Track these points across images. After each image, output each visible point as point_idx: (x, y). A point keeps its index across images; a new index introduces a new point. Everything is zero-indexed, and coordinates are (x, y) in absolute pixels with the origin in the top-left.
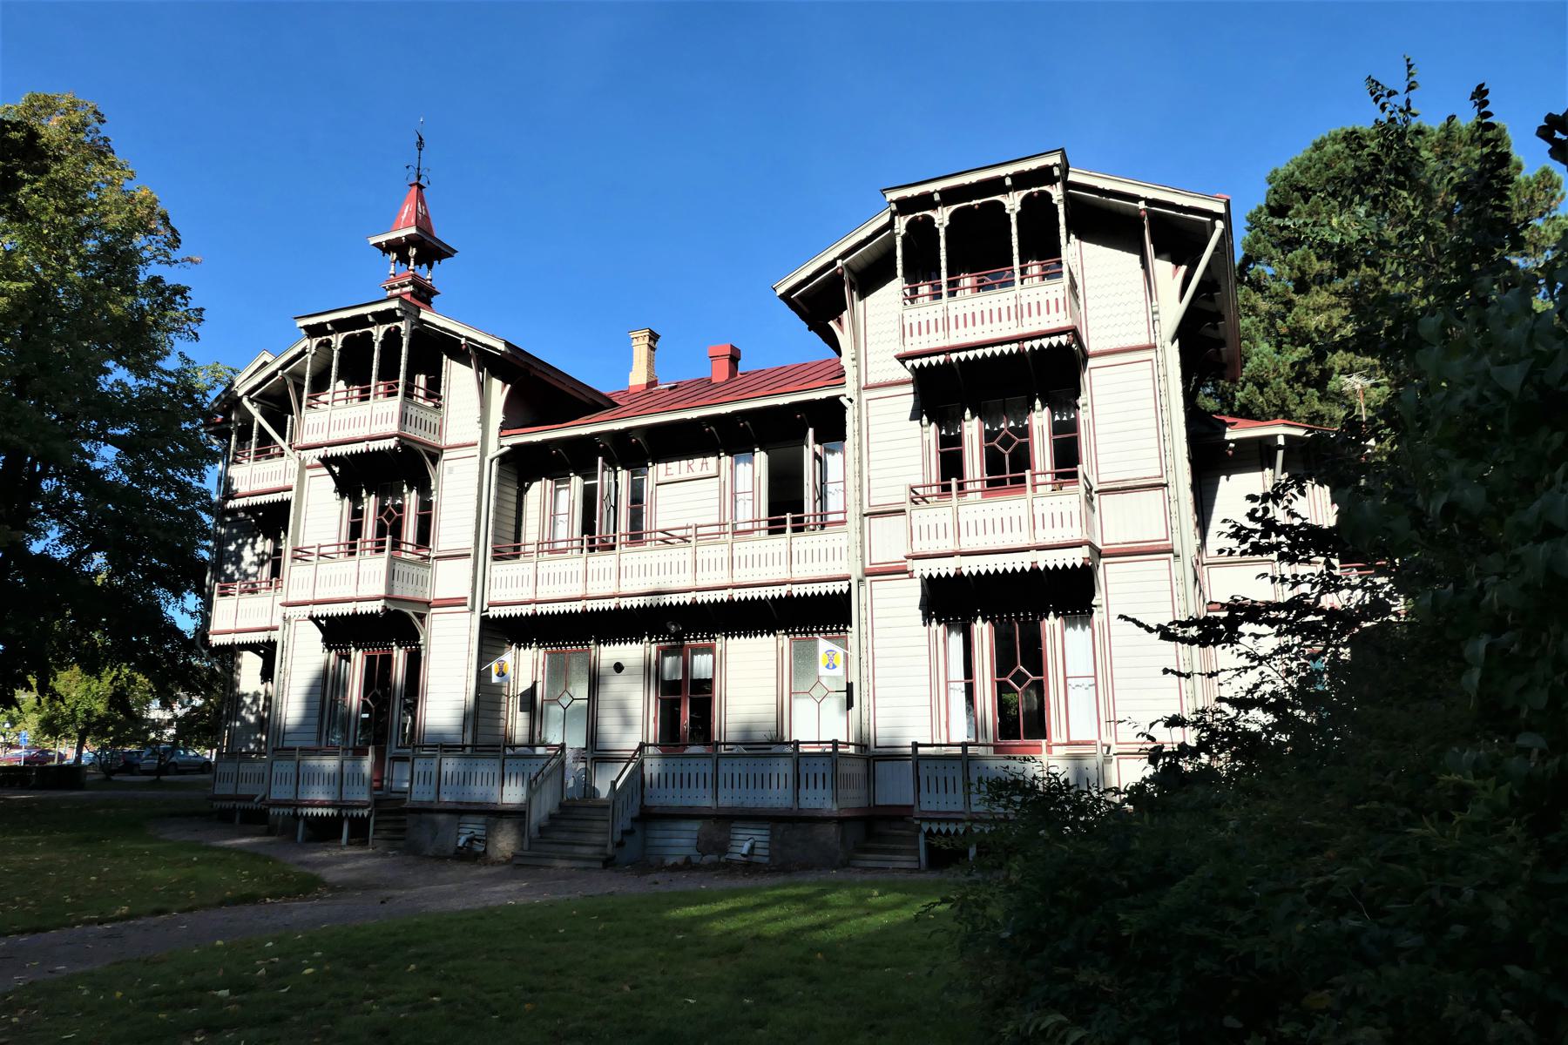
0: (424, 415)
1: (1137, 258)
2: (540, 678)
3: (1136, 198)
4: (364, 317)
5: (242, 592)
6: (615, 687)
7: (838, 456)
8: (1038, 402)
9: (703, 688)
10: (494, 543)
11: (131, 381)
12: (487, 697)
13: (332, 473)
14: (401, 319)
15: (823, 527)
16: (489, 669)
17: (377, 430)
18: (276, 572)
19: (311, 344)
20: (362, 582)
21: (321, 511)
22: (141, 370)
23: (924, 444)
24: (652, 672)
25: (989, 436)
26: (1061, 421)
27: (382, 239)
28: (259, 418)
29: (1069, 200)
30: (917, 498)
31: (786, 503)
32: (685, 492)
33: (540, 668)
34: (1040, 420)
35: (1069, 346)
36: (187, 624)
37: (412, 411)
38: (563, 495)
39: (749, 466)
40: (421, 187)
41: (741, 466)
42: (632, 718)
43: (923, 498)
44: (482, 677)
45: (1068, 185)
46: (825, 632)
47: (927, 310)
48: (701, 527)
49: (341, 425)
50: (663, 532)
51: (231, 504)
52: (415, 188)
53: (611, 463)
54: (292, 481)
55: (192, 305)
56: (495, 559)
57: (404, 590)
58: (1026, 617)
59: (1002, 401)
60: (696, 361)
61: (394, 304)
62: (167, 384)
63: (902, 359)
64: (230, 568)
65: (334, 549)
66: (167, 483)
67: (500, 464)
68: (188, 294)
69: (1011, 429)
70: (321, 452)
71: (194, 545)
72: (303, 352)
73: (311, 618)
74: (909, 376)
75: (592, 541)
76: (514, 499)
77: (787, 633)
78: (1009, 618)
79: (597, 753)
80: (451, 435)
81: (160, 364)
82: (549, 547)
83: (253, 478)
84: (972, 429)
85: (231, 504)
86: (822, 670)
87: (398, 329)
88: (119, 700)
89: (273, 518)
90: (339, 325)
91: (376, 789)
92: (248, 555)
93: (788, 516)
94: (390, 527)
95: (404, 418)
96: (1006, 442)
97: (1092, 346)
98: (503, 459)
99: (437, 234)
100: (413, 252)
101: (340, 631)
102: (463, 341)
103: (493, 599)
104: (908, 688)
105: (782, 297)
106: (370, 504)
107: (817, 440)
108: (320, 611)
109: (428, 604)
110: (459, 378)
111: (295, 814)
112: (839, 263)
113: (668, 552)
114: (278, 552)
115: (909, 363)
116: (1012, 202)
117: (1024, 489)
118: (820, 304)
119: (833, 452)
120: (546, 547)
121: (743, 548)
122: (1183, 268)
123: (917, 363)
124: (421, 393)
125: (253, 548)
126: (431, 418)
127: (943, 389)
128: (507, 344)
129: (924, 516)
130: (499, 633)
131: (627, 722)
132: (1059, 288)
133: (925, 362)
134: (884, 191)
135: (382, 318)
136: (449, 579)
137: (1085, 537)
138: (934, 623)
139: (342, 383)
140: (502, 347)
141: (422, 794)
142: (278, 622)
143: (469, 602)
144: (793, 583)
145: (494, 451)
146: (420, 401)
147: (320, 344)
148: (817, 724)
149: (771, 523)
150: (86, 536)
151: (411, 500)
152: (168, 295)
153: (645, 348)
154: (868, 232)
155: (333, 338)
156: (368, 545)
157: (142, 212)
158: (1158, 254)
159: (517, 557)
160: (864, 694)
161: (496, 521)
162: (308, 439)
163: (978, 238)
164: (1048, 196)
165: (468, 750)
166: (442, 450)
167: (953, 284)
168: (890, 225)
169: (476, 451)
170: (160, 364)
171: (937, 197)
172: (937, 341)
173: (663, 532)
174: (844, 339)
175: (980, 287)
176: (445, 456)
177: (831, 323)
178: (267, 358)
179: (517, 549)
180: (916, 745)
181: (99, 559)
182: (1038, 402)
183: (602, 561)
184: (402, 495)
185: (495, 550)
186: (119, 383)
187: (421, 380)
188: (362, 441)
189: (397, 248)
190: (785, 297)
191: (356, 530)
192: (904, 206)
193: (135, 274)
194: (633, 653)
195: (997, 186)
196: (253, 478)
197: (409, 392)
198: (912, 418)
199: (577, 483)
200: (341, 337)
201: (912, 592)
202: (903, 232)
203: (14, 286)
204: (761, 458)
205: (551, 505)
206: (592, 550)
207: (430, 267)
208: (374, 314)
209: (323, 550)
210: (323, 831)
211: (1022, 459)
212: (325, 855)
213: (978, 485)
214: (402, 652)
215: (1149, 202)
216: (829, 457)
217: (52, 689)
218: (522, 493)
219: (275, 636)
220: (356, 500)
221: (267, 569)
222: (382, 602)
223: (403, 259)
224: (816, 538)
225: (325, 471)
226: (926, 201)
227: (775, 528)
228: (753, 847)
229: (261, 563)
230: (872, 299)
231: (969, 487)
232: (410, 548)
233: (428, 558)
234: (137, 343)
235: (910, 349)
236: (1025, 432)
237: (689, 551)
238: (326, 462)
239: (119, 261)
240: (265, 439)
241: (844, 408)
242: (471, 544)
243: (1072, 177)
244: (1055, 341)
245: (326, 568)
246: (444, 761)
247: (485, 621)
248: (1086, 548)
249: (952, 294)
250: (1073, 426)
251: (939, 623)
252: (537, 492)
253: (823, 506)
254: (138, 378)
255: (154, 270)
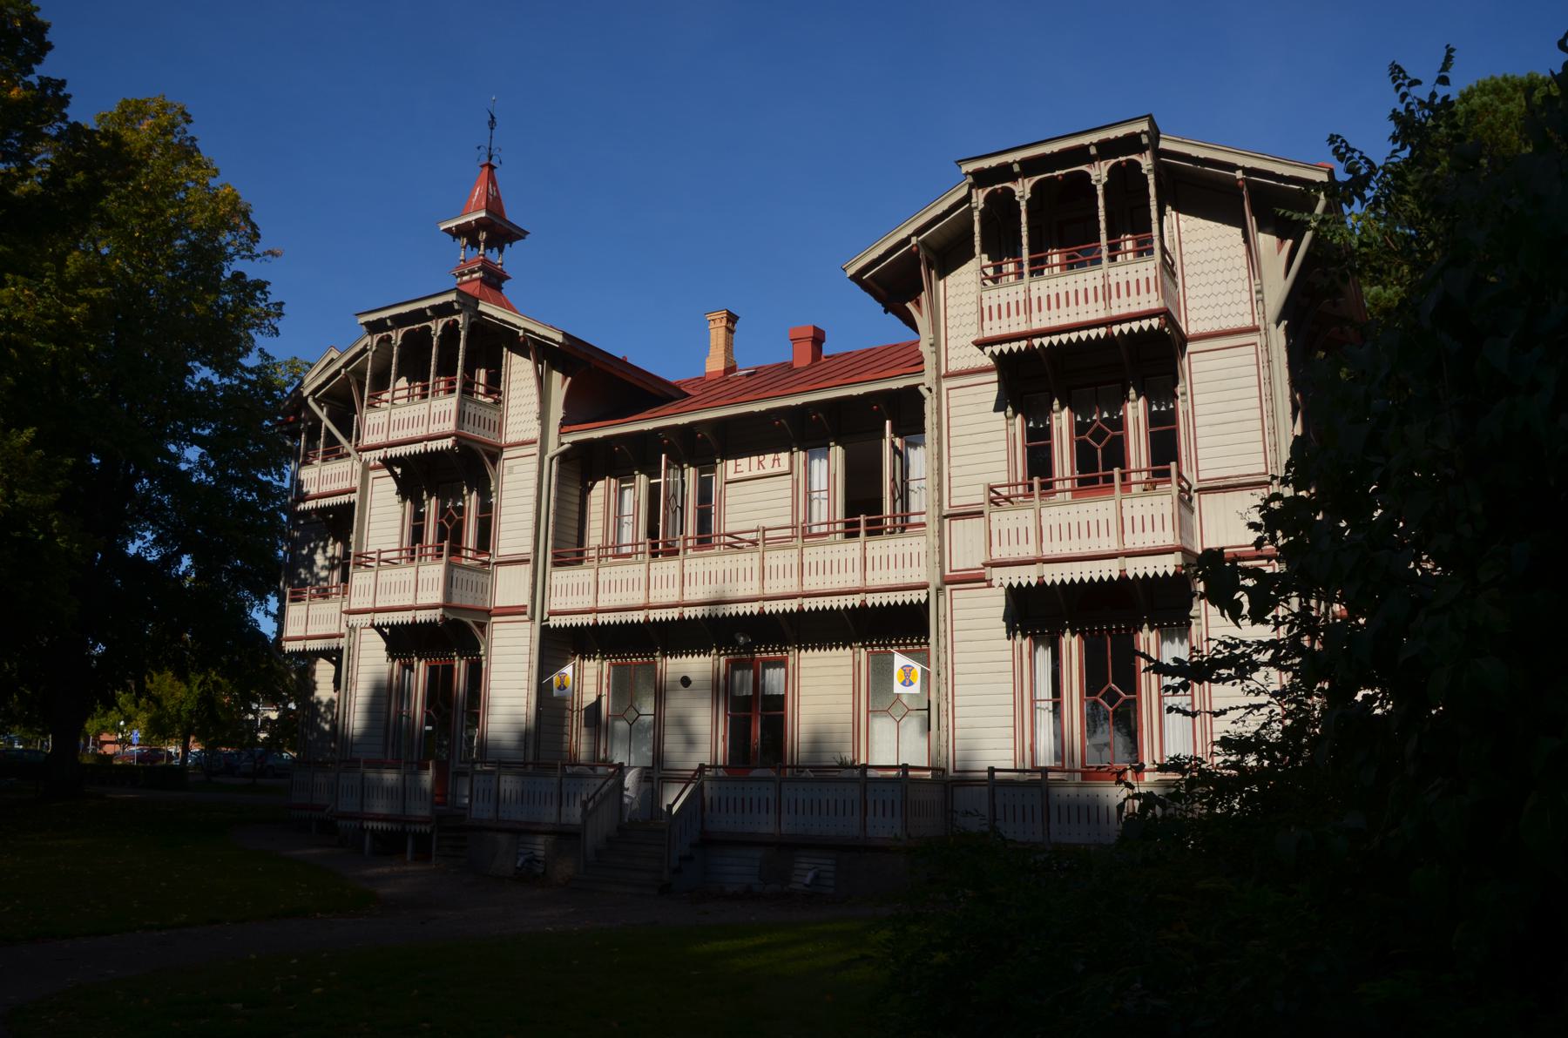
0: (482, 412)
1: (1239, 231)
2: (604, 691)
3: (1234, 167)
4: (423, 311)
5: (312, 597)
6: (677, 703)
7: (920, 450)
8: (1132, 391)
9: (776, 705)
10: (554, 547)
11: (215, 379)
12: (550, 705)
13: (394, 474)
14: (458, 312)
15: (903, 529)
16: (551, 681)
17: (435, 429)
18: (345, 578)
19: (371, 341)
20: (418, 589)
21: (384, 516)
22: (225, 368)
23: (1011, 440)
24: (721, 689)
25: (1079, 429)
26: (1159, 411)
27: (452, 224)
28: (326, 422)
29: (1159, 169)
30: (996, 498)
31: (865, 507)
32: (756, 491)
33: (605, 681)
34: (1135, 411)
35: (1161, 330)
36: (268, 627)
37: (470, 408)
38: (628, 494)
39: (824, 462)
40: (492, 168)
41: (816, 462)
42: (703, 735)
43: (1007, 499)
44: (543, 690)
45: (1158, 154)
46: (898, 645)
47: (1010, 292)
48: (772, 530)
49: (401, 424)
50: (730, 535)
51: (302, 506)
52: (486, 169)
53: (677, 461)
54: (356, 483)
55: (272, 299)
56: (555, 564)
57: (463, 598)
58: (1119, 629)
59: (1101, 393)
60: (769, 347)
61: (452, 297)
62: (249, 382)
63: (981, 344)
64: (303, 573)
65: (396, 554)
66: (251, 483)
67: (560, 463)
68: (268, 289)
69: (1104, 421)
70: (380, 453)
71: (275, 547)
72: (364, 350)
73: (372, 626)
74: (989, 362)
75: (655, 546)
76: (577, 500)
77: (864, 646)
78: (1101, 630)
79: (657, 773)
80: (512, 433)
81: (242, 361)
82: (614, 551)
83: (322, 479)
84: (1062, 421)
85: (302, 506)
86: (898, 688)
87: (456, 322)
88: (207, 701)
89: (339, 520)
90: (399, 320)
91: (438, 804)
92: (320, 559)
93: (862, 518)
94: (451, 533)
95: (461, 416)
96: (1099, 435)
97: (1193, 323)
98: (564, 457)
99: (510, 216)
100: (483, 236)
101: (403, 640)
102: (521, 333)
103: (553, 608)
104: (990, 706)
105: (853, 278)
106: (431, 507)
107: (896, 432)
108: (381, 619)
109: (488, 613)
110: (520, 372)
111: (361, 827)
112: (914, 240)
113: (735, 557)
114: (347, 555)
115: (988, 350)
116: (1099, 172)
117: (1113, 491)
118: (898, 284)
119: (915, 445)
120: (610, 551)
121: (813, 554)
122: (1289, 242)
123: (996, 349)
124: (481, 389)
125: (325, 551)
126: (490, 415)
127: (1032, 377)
128: (565, 335)
129: (1004, 520)
130: (560, 644)
131: (690, 741)
132: (1149, 268)
133: (1006, 348)
134: (960, 162)
135: (441, 311)
136: (510, 587)
137: (1178, 542)
138: (1019, 637)
139: (404, 379)
140: (559, 338)
141: (482, 811)
142: (344, 630)
143: (529, 611)
144: (867, 592)
145: (553, 449)
146: (480, 398)
147: (381, 341)
148: (893, 746)
149: (848, 525)
150: (175, 538)
151: (472, 502)
152: (249, 290)
153: (722, 331)
154: (945, 206)
155: (393, 334)
156: (430, 550)
157: (224, 209)
158: (1260, 229)
159: (580, 562)
160: (943, 713)
161: (556, 524)
162: (368, 439)
163: (1062, 213)
164: (1138, 165)
165: (530, 768)
166: (501, 449)
167: (1114, 248)
168: (967, 198)
169: (535, 449)
170: (242, 361)
171: (1016, 168)
172: (1018, 325)
173: (730, 535)
174: (922, 321)
175: (1070, 265)
176: (505, 455)
177: (909, 305)
178: (334, 355)
179: (581, 553)
180: (992, 770)
181: (186, 561)
182: (1132, 391)
183: (666, 568)
184: (463, 497)
185: (555, 555)
186: (205, 381)
187: (482, 375)
188: (420, 441)
189: (467, 233)
190: (856, 278)
191: (417, 534)
192: (981, 179)
193: (220, 271)
194: (698, 666)
195: (1080, 155)
196: (322, 479)
197: (468, 389)
198: (996, 410)
199: (642, 480)
200: (401, 332)
201: (992, 603)
202: (981, 206)
203: (94, 293)
204: (837, 453)
205: (614, 506)
206: (654, 555)
207: (501, 251)
208: (432, 308)
209: (384, 556)
210: (390, 844)
211: (1117, 455)
212: (386, 870)
213: (1068, 484)
214: (422, 663)
215: (1246, 171)
216: (911, 452)
217: (149, 692)
218: (585, 492)
219: (343, 643)
220: (418, 503)
221: (336, 575)
222: (440, 611)
223: (474, 243)
224: (892, 542)
225: (386, 472)
226: (1005, 173)
227: (851, 533)
228: (817, 877)
229: (332, 568)
230: (949, 279)
231: (1134, 477)
232: (470, 554)
233: (488, 563)
234: (223, 343)
235: (988, 334)
236: (1120, 424)
237: (756, 556)
238: (388, 463)
239: (207, 257)
240: (331, 440)
241: (922, 399)
242: (529, 549)
243: (1163, 145)
244: (1145, 324)
245: (388, 575)
246: (502, 778)
247: (546, 632)
248: (1179, 554)
249: (1113, 259)
250: (1171, 417)
251: (1024, 637)
252: (600, 492)
253: (906, 505)
254: (221, 377)
255: (238, 265)
